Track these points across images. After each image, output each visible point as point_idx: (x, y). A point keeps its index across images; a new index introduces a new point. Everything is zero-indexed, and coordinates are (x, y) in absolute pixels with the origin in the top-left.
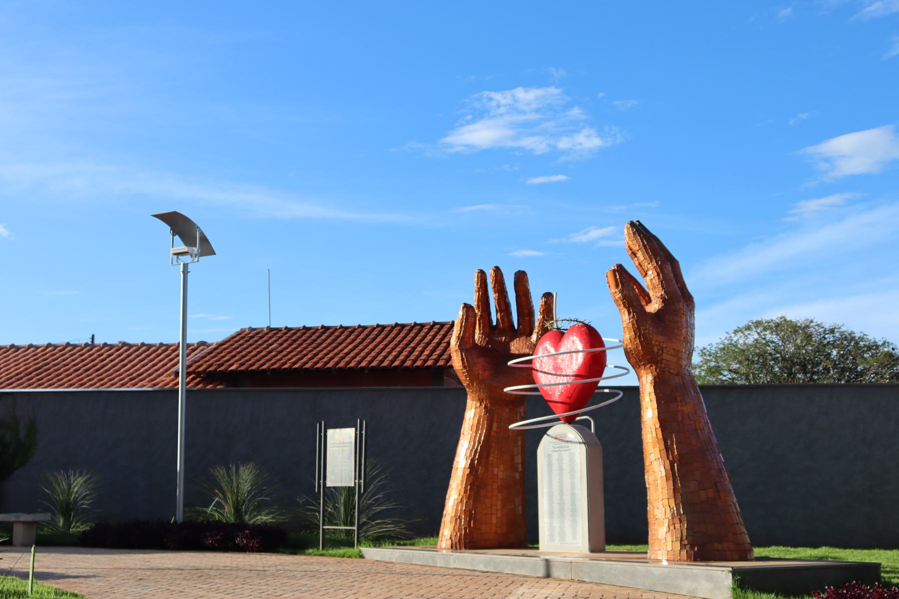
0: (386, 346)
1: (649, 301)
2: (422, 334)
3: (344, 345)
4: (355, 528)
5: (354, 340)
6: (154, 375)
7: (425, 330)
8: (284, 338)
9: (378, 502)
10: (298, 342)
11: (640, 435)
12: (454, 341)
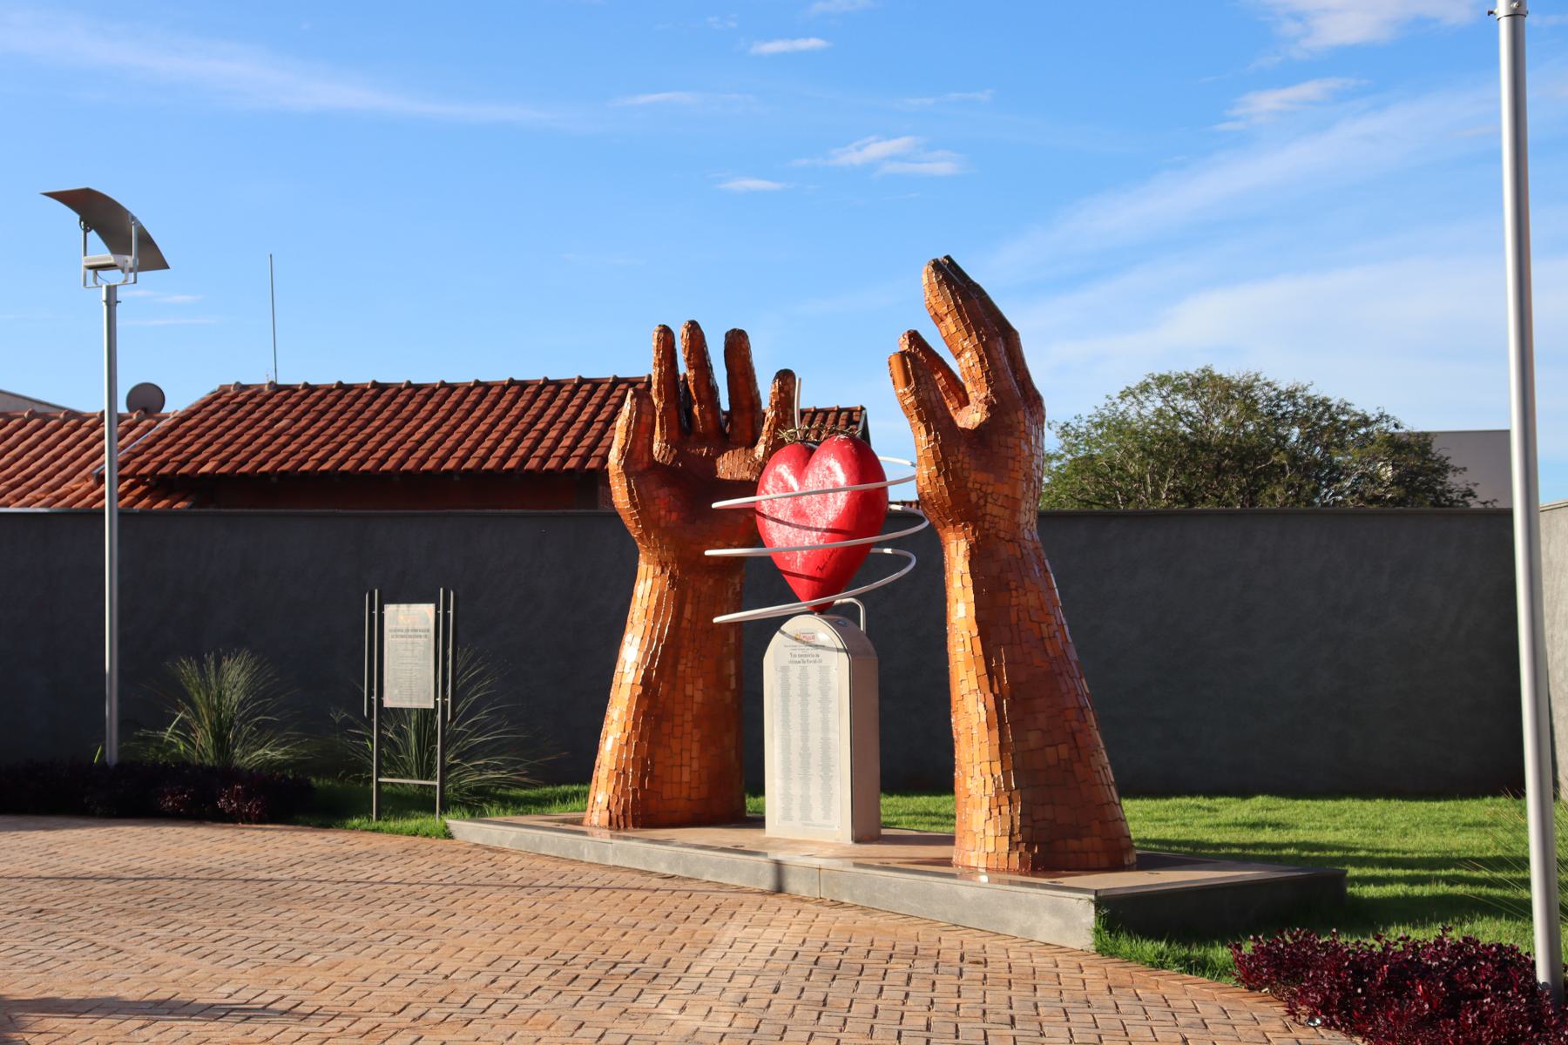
0: (493, 426)
1: (964, 401)
2: (558, 402)
3: (414, 423)
4: (437, 783)
5: (433, 413)
6: (56, 478)
7: (564, 395)
8: (302, 407)
9: (480, 729)
10: (330, 415)
11: (945, 645)
12: (614, 457)
